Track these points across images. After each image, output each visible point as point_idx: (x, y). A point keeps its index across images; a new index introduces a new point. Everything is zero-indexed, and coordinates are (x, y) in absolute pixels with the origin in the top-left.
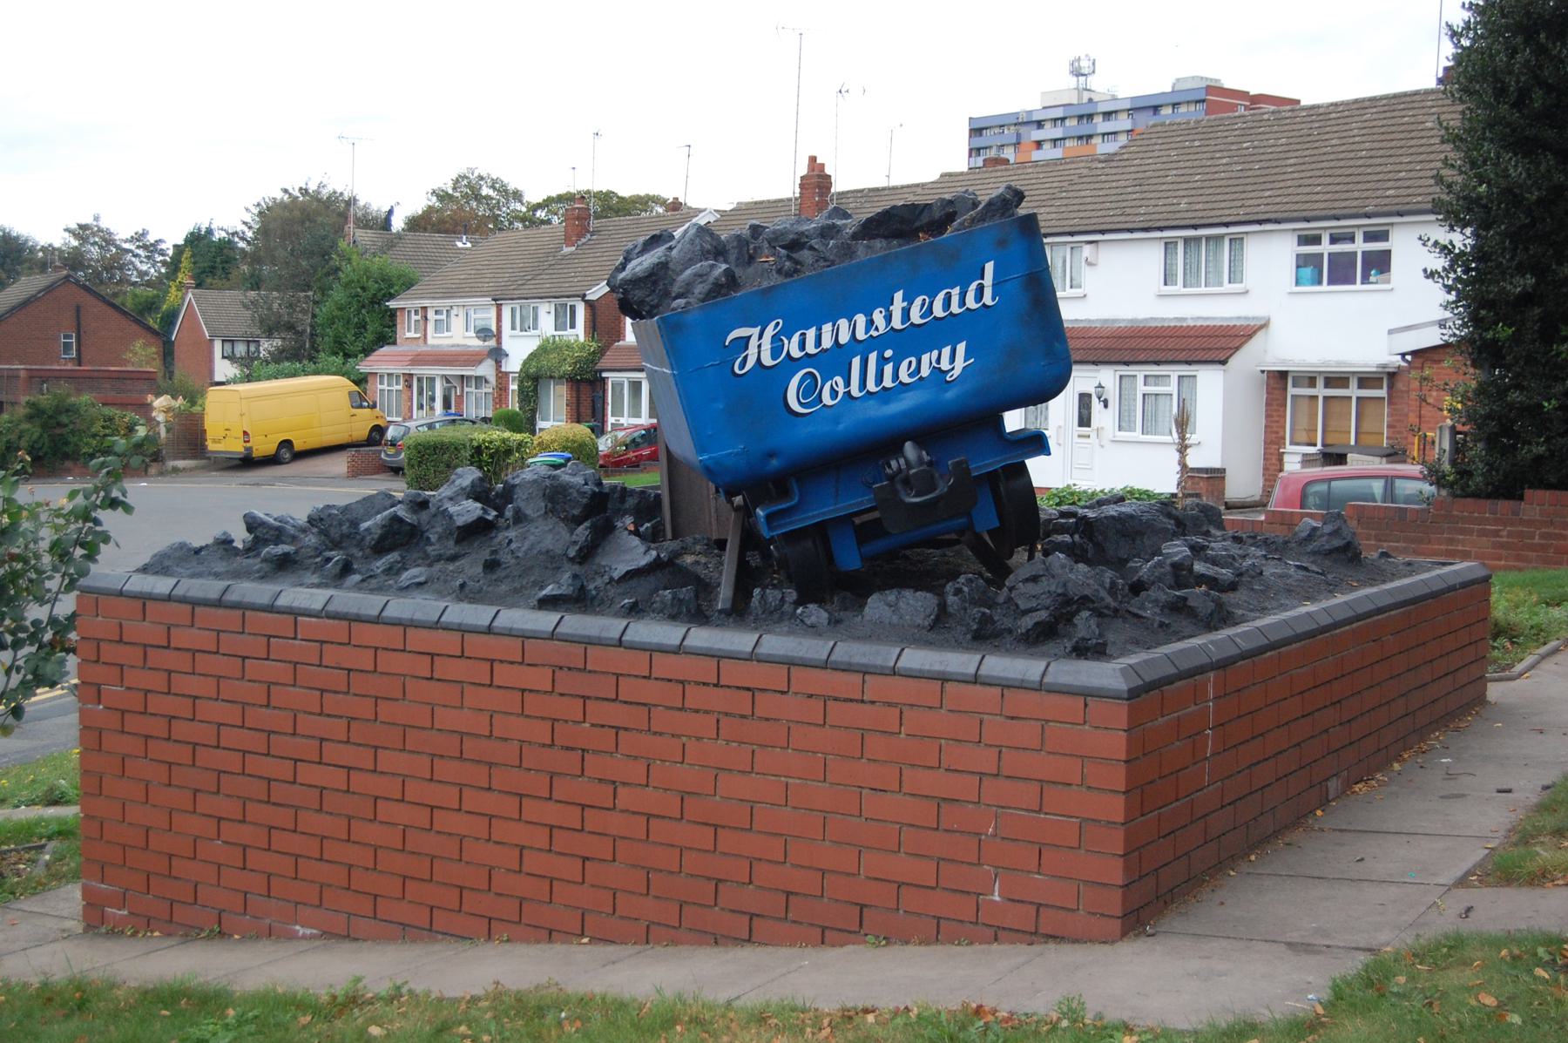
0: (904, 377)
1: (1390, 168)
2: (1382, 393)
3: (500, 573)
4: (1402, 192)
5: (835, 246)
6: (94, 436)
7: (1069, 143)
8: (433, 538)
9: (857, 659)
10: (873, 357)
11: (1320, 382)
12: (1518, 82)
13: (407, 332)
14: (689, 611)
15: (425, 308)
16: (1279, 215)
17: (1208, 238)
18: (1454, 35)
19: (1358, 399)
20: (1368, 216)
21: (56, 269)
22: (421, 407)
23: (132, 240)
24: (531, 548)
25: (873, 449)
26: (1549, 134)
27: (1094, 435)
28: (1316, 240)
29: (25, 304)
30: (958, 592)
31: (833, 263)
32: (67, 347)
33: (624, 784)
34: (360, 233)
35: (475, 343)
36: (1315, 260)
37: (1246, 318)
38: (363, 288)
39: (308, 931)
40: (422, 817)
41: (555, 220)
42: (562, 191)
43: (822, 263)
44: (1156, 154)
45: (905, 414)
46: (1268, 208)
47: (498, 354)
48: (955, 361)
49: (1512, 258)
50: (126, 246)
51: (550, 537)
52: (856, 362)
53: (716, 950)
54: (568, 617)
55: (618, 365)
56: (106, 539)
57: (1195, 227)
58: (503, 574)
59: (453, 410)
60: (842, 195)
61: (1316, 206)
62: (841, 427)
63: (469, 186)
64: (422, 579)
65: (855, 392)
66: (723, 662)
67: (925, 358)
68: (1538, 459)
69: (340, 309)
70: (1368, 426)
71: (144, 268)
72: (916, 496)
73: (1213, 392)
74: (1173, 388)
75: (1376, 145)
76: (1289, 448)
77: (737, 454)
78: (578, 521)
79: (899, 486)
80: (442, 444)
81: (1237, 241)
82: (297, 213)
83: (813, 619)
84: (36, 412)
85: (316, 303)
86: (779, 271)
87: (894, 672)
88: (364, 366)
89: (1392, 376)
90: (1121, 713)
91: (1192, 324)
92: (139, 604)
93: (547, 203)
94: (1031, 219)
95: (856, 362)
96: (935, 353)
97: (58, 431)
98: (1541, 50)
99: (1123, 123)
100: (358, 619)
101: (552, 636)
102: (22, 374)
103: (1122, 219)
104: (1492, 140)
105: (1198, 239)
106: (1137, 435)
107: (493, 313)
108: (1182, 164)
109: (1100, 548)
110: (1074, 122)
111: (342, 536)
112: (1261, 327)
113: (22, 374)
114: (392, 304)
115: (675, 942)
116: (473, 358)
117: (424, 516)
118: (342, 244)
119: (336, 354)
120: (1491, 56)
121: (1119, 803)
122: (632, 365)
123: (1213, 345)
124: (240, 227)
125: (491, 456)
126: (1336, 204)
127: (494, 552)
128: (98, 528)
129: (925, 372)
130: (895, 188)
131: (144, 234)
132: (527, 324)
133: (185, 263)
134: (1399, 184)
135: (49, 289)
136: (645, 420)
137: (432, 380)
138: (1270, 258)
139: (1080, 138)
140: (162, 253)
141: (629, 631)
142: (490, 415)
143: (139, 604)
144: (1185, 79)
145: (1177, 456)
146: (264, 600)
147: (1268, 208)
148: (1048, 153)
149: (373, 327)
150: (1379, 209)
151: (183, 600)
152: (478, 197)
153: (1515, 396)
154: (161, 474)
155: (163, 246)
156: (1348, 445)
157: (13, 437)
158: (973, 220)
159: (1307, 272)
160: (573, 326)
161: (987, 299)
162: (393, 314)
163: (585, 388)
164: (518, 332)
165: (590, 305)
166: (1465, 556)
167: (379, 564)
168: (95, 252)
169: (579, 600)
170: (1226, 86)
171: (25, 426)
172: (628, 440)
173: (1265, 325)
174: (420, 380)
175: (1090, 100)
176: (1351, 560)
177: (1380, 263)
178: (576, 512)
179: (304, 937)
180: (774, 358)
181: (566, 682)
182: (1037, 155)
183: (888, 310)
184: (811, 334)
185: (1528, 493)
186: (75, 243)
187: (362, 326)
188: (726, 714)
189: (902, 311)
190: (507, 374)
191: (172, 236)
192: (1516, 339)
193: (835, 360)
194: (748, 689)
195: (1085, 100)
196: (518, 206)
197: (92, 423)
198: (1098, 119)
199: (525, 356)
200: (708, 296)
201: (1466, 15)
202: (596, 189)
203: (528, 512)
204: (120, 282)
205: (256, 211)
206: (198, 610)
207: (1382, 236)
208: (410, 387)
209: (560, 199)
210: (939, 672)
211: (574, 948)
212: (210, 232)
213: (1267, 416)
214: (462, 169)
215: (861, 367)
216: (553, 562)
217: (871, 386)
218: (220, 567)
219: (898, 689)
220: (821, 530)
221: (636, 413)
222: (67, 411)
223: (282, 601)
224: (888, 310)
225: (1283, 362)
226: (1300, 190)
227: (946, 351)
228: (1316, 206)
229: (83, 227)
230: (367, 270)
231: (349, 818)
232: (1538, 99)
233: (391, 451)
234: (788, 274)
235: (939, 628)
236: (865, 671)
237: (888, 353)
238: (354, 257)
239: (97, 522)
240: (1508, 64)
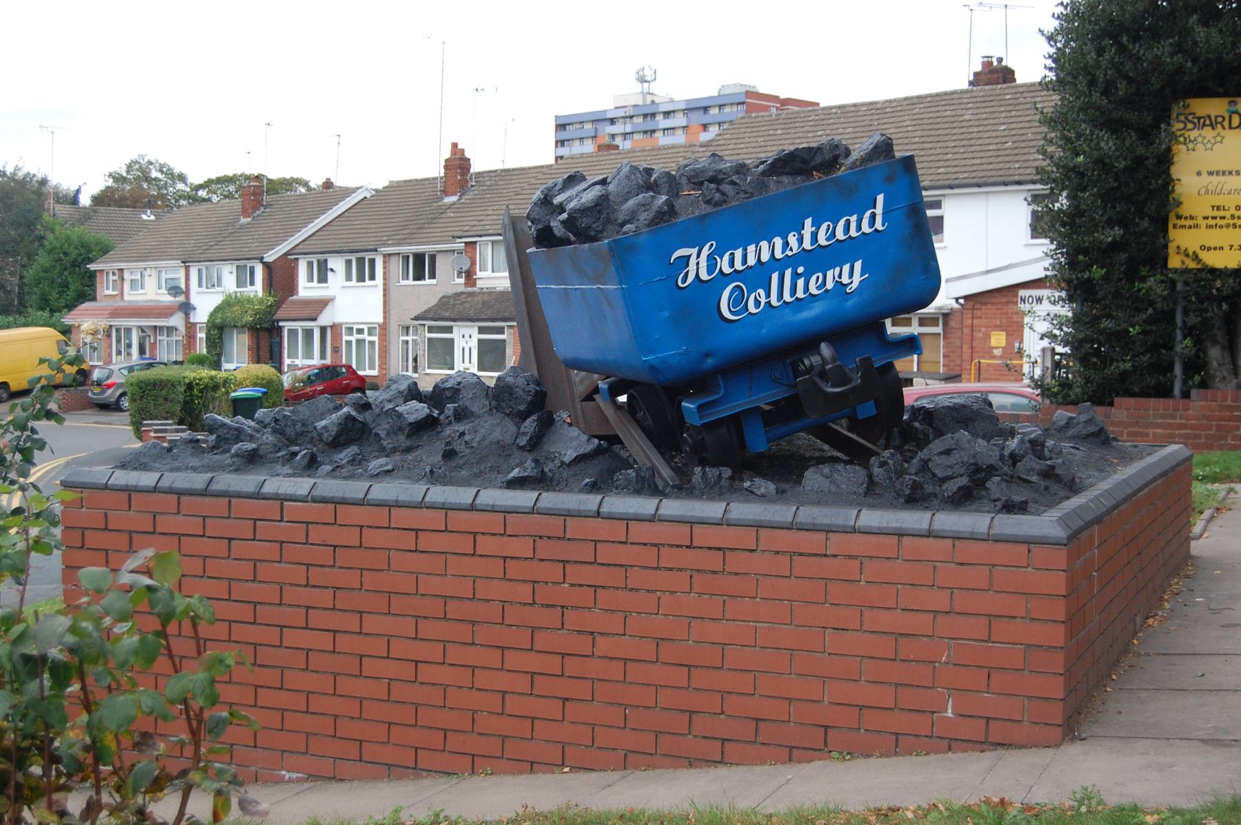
1: (939, 151)
3: (458, 461)
4: (950, 170)
7: (636, 137)
8: (383, 434)
9: (820, 520)
10: (788, 273)
12: (1105, 75)
13: (106, 290)
15: (121, 270)
18: (1051, 38)
22: (119, 353)
24: (484, 438)
26: (1132, 116)
30: (883, 464)
31: (752, 195)
33: (601, 634)
34: (58, 207)
35: (166, 298)
38: (66, 254)
39: (294, 775)
40: (407, 670)
41: (215, 198)
42: (221, 174)
44: (747, 140)
45: (815, 319)
47: (187, 308)
48: (853, 276)
49: (1102, 215)
51: (499, 429)
52: (775, 277)
53: (692, 771)
54: (544, 494)
55: (293, 316)
56: (42, 445)
58: (461, 462)
59: (147, 355)
60: (479, 174)
62: (764, 331)
64: (389, 467)
65: (774, 302)
66: (695, 527)
67: (830, 274)
68: (1125, 374)
69: (45, 271)
72: (832, 386)
75: (925, 133)
77: (680, 354)
78: (523, 416)
79: (817, 380)
80: (161, 381)
83: (763, 490)
85: (24, 266)
86: (708, 202)
87: (854, 530)
88: (68, 320)
90: (1060, 557)
92: (125, 495)
93: (207, 185)
95: (775, 277)
96: (838, 269)
98: (1122, 49)
99: (679, 120)
100: (344, 502)
101: (533, 511)
104: (1084, 121)
107: (181, 274)
110: (640, 120)
111: (297, 434)
114: (92, 267)
115: (654, 767)
116: (166, 312)
117: (367, 416)
118: (46, 217)
119: (42, 309)
120: (1083, 55)
121: (1060, 630)
122: (305, 316)
125: (201, 391)
127: (448, 444)
128: (35, 436)
130: (508, 170)
132: (214, 283)
134: (948, 163)
136: (316, 361)
137: (128, 330)
139: (645, 132)
141: (604, 504)
142: (180, 359)
143: (125, 495)
144: (729, 86)
146: (251, 488)
149: (74, 286)
151: (170, 491)
152: (148, 179)
153: (1105, 324)
156: (912, 372)
160: (252, 283)
161: (879, 225)
162: (92, 275)
163: (264, 335)
164: (204, 289)
165: (268, 267)
166: (1169, 440)
167: (341, 455)
169: (540, 481)
170: (761, 91)
172: (305, 377)
174: (118, 330)
175: (653, 102)
176: (1103, 443)
178: (522, 408)
179: (290, 781)
180: (709, 274)
181: (545, 549)
183: (800, 234)
184: (738, 253)
185: (1117, 400)
187: (65, 286)
188: (698, 571)
189: (811, 234)
190: (195, 324)
192: (1106, 278)
193: (758, 275)
194: (719, 549)
195: (649, 102)
196: (180, 186)
198: (660, 118)
199: (211, 309)
201: (1056, 23)
203: (475, 409)
206: (183, 498)
208: (109, 336)
209: (219, 180)
210: (896, 529)
211: (558, 776)
214: (134, 156)
215: (779, 279)
216: (504, 450)
218: (194, 462)
219: (856, 543)
220: (735, 420)
221: (308, 355)
223: (267, 489)
224: (800, 234)
227: (846, 268)
230: (68, 240)
231: (335, 675)
232: (1122, 88)
233: (97, 390)
234: (717, 204)
235: (871, 493)
236: (828, 530)
237: (801, 270)
238: (57, 227)
239: (33, 431)
240: (1097, 61)
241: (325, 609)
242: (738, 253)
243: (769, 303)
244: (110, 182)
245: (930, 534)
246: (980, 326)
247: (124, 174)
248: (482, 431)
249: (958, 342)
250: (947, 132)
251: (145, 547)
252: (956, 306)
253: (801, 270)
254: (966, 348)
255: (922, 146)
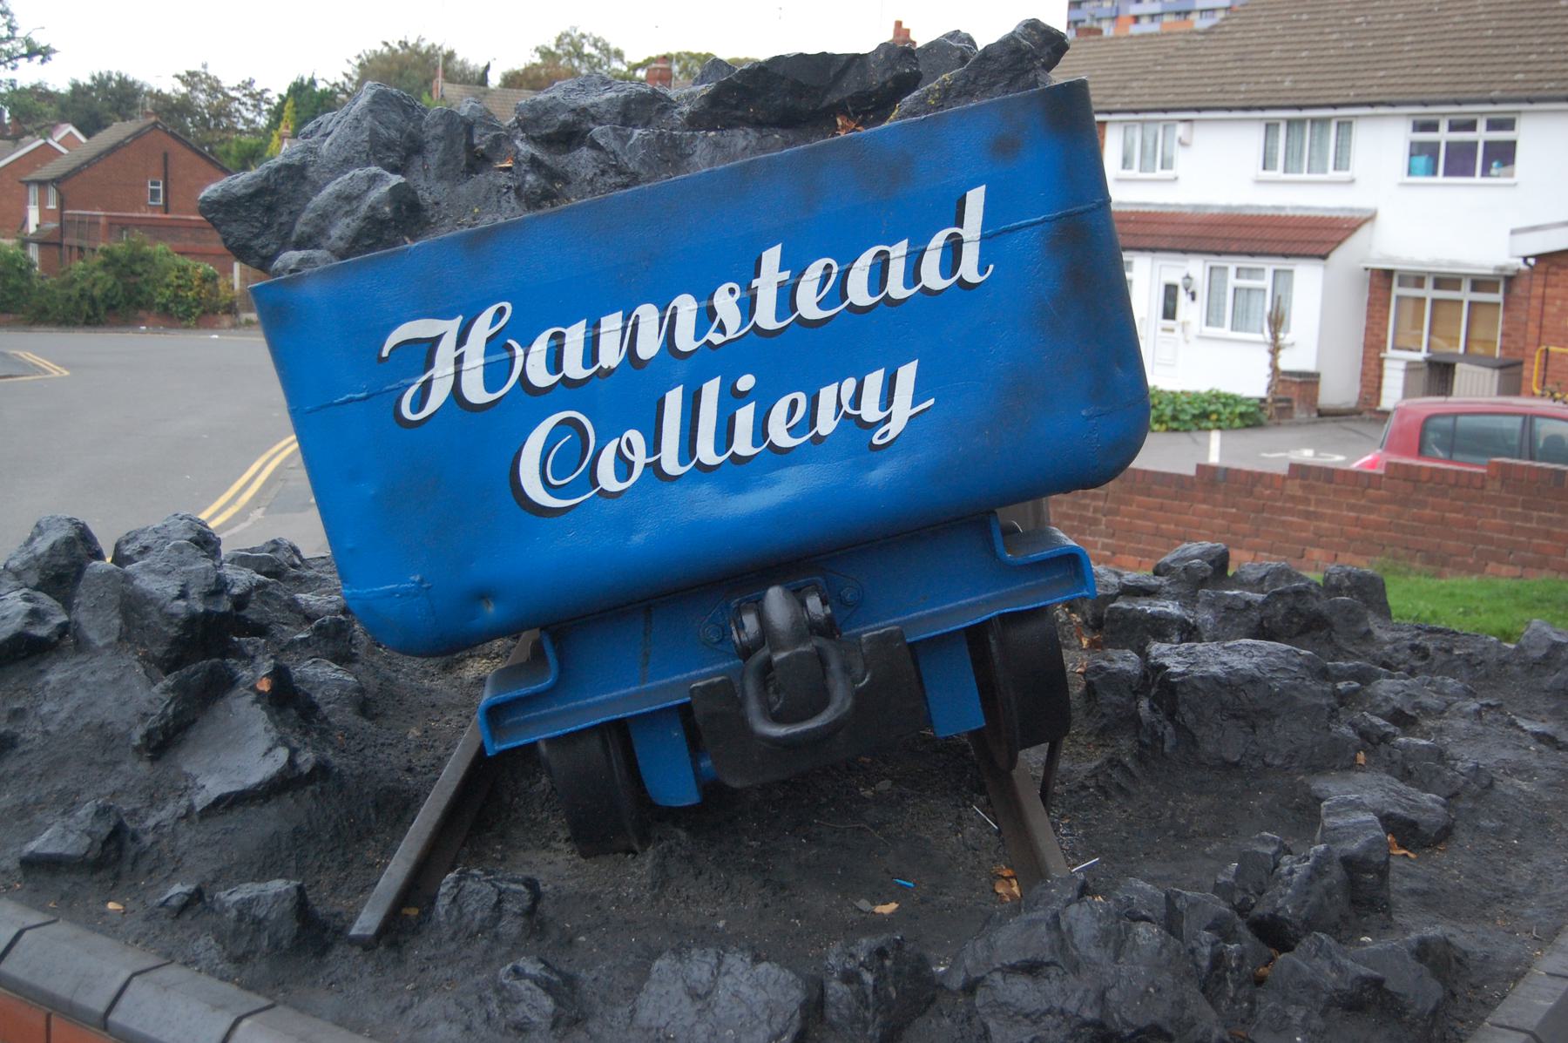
0: (779, 434)
1: (1518, 49)
2: (1498, 297)
4: (1532, 76)
5: (645, 143)
6: (168, 286)
7: (1166, 19)
10: (711, 391)
11: (1429, 283)
14: (275, 945)
16: (1425, 97)
17: (1313, 121)
19: (1471, 303)
20: (1493, 102)
21: (147, 115)
23: (238, 88)
25: (713, 583)
27: (1178, 330)
28: (1432, 127)
29: (114, 149)
31: (635, 179)
32: (155, 193)
36: (1430, 150)
37: (1352, 210)
43: (611, 179)
44: (1261, 27)
46: (1381, 90)
48: (893, 401)
50: (233, 94)
52: (674, 400)
57: (1300, 108)
61: (1435, 89)
62: (637, 539)
63: (572, 43)
65: (670, 462)
67: (827, 395)
70: (1479, 333)
71: (250, 116)
73: (1310, 287)
74: (1267, 282)
76: (1390, 352)
77: (406, 594)
81: (1345, 125)
82: (396, 67)
84: (111, 261)
89: (1510, 280)
91: (1290, 213)
94: (1076, 92)
95: (674, 400)
96: (849, 385)
97: (132, 280)
102: (102, 221)
103: (1220, 96)
105: (1302, 121)
106: (1225, 331)
108: (1288, 39)
109: (1188, 738)
112: (1366, 221)
113: (102, 221)
123: (1314, 238)
124: (341, 79)
126: (1459, 88)
129: (826, 424)
131: (251, 83)
133: (288, 112)
135: (137, 135)
138: (1381, 144)
139: (1178, 13)
140: (268, 102)
145: (1267, 358)
147: (1381, 90)
148: (1146, 27)
150: (1505, 95)
152: (580, 56)
154: (234, 326)
155: (267, 95)
157: (86, 285)
158: (945, 92)
159: (1422, 161)
161: (969, 269)
168: (202, 98)
171: (99, 274)
173: (1369, 218)
177: (1503, 154)
180: (490, 386)
182: (1135, 30)
184: (575, 335)
186: (184, 90)
189: (776, 290)
191: (277, 87)
193: (629, 394)
196: (616, 65)
197: (166, 273)
200: (356, 244)
202: (695, 51)
203: (93, 635)
204: (227, 129)
205: (357, 62)
207: (1508, 125)
212: (313, 82)
213: (1369, 317)
217: (706, 452)
220: (620, 731)
222: (142, 259)
225: (1390, 259)
226: (1418, 71)
227: (874, 381)
228: (1435, 89)
229: (192, 74)
237: (746, 383)
242: (575, 335)
243: (655, 468)
244: (537, 59)
246: (1555, 298)
247: (553, 49)
248: (80, 693)
249: (1524, 317)
250: (1533, 23)
252: (1523, 267)
253: (746, 383)
254: (1533, 327)
255: (1496, 42)
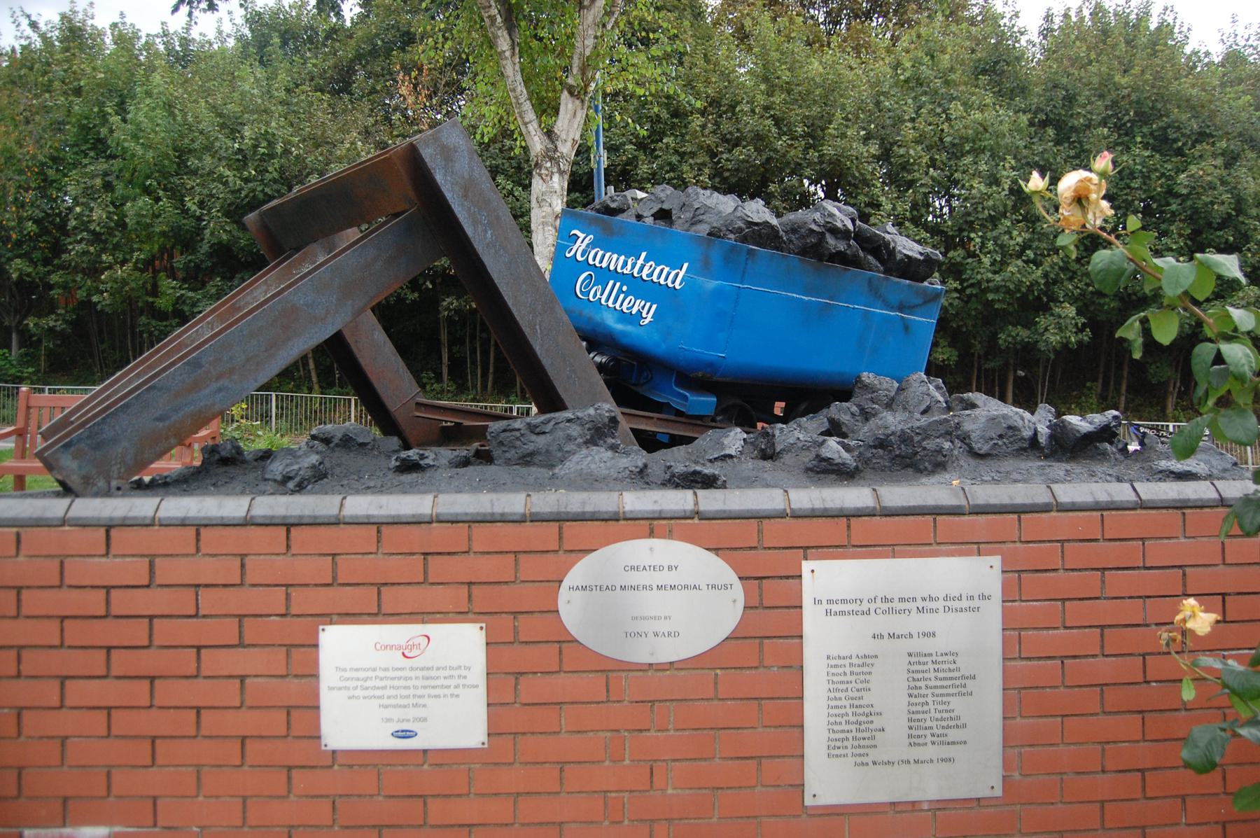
52: (611, 282)
65: (603, 302)
95: (611, 282)
227: (648, 305)
241: (119, 766)
245: (247, 522)
251: (1074, 430)
253: (625, 288)
